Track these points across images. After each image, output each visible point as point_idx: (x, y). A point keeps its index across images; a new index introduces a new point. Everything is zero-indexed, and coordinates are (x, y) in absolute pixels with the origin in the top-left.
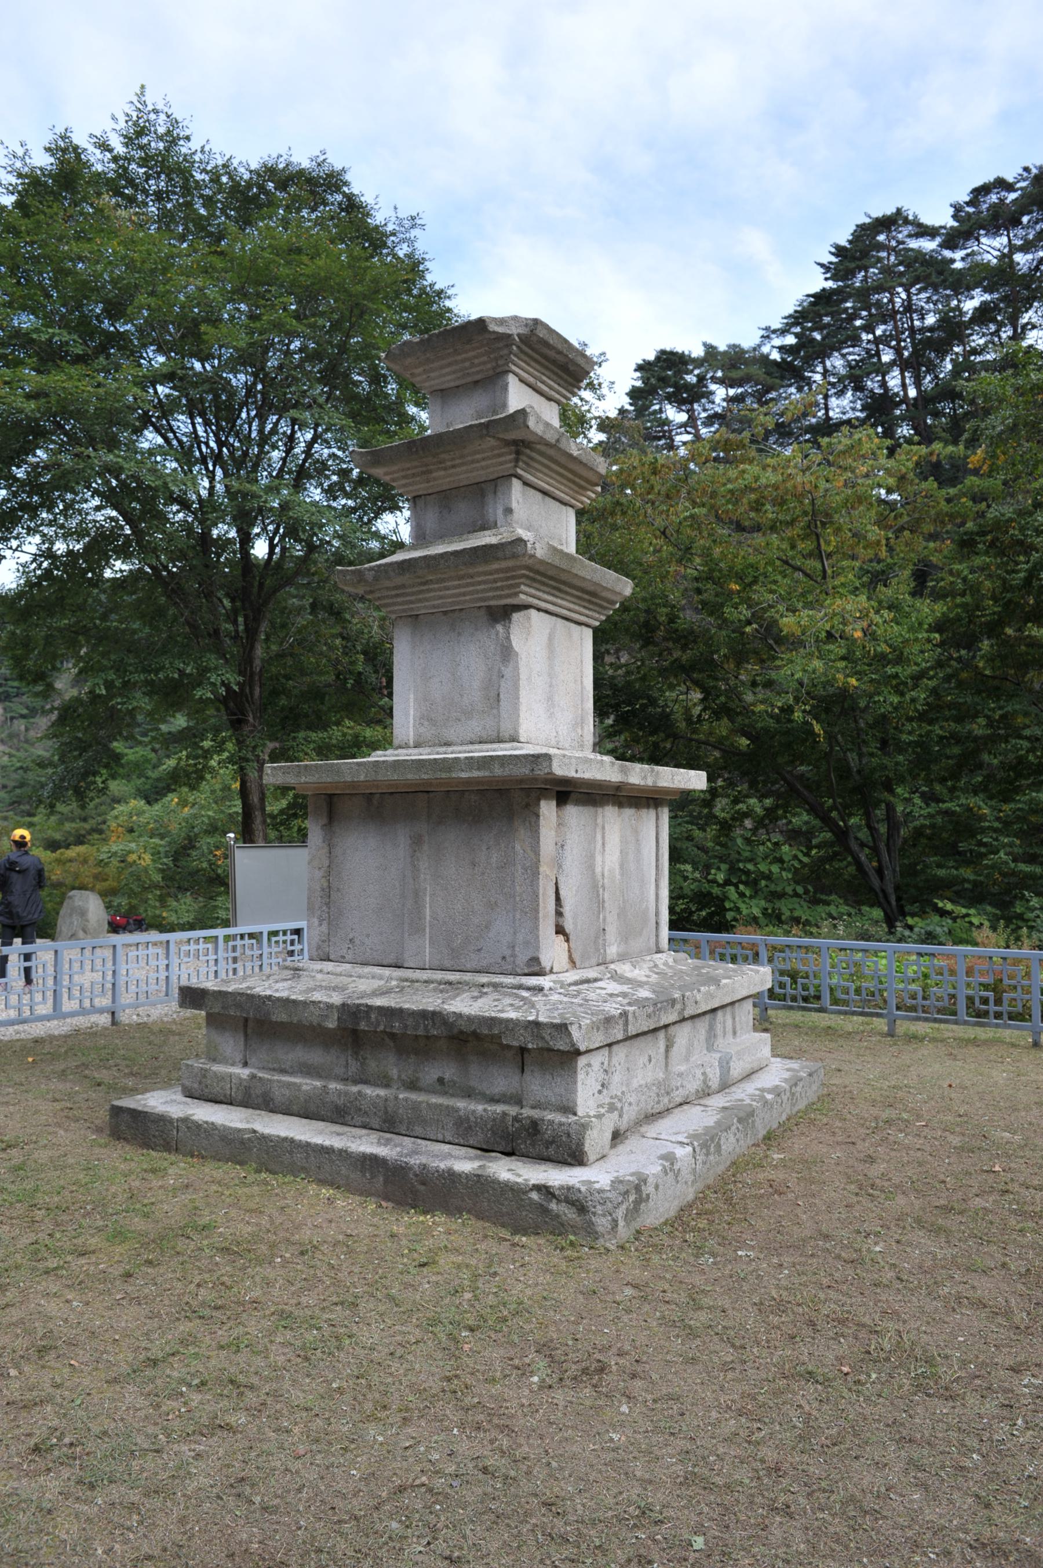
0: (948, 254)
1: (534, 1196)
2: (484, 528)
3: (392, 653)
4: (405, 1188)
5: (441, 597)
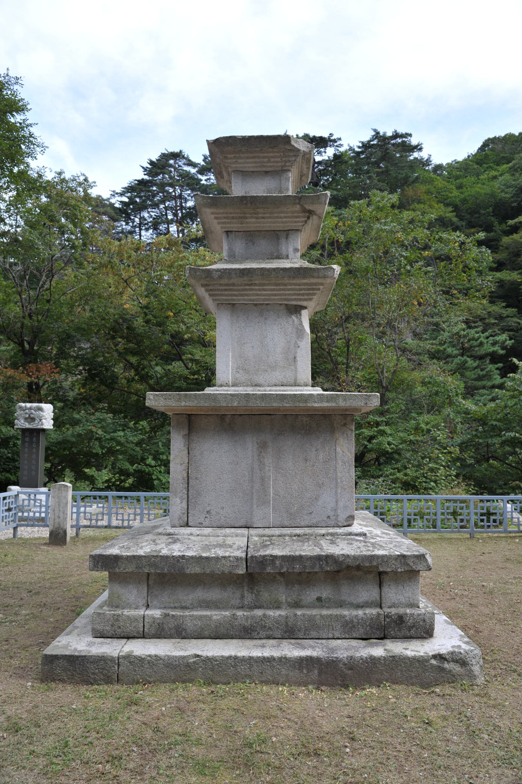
0: (200, 176)
1: (433, 662)
2: (279, 257)
4: (332, 675)
5: (258, 295)
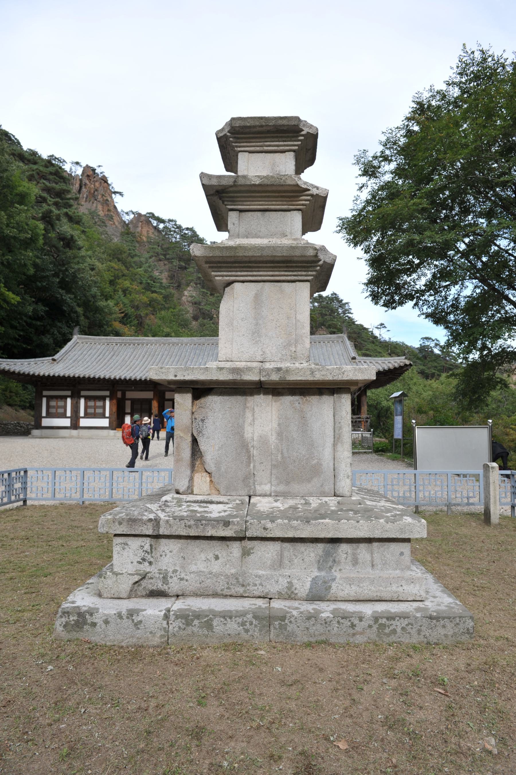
3: (218, 317)
